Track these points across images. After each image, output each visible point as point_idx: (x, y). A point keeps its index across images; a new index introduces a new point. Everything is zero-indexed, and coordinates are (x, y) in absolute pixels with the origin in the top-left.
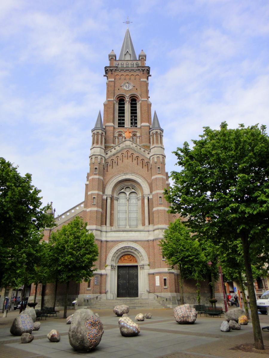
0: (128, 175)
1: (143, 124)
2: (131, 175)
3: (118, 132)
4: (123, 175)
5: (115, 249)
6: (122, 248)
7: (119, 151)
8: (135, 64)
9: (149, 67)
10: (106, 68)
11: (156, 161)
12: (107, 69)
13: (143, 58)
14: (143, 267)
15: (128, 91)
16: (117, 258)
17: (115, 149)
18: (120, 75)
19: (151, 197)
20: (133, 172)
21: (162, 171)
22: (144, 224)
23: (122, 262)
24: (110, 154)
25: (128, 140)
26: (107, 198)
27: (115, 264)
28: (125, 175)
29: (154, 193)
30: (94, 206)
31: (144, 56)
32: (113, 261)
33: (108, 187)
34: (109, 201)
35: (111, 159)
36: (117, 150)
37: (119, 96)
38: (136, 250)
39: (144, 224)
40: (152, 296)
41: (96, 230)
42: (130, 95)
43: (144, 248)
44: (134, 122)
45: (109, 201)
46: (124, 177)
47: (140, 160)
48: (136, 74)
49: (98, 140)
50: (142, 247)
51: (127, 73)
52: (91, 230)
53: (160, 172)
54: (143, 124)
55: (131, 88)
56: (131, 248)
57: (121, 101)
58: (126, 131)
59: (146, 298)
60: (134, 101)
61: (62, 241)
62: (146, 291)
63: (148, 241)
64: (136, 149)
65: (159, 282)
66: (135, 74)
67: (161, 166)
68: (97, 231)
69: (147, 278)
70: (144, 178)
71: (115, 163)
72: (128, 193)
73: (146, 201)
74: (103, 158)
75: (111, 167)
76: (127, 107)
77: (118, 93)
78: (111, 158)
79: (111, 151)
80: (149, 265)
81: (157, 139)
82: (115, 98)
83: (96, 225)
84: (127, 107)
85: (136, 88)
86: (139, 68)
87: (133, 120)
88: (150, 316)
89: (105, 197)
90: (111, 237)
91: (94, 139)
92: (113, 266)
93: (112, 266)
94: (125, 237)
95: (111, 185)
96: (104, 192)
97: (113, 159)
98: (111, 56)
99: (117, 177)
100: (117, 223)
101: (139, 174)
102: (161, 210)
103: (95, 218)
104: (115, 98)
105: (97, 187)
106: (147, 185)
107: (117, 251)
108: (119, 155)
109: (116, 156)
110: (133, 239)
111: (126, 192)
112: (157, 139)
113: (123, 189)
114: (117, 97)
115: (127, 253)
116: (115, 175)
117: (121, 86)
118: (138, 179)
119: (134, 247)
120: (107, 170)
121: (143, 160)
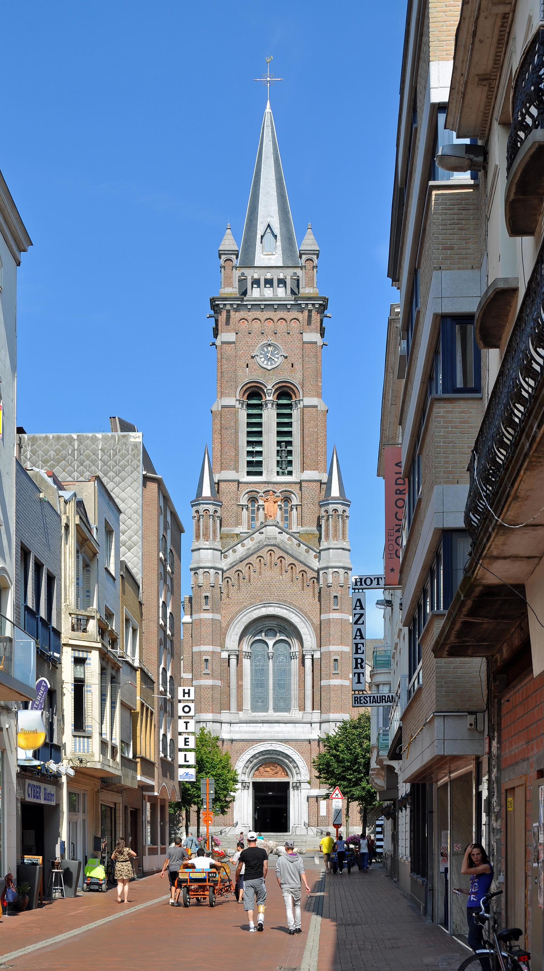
0: (271, 606)
1: (309, 474)
2: (279, 607)
3: (247, 493)
4: (262, 607)
5: (247, 753)
6: (261, 752)
7: (251, 552)
8: (289, 278)
9: (325, 298)
10: (213, 300)
11: (331, 582)
12: (216, 303)
13: (311, 260)
14: (297, 786)
15: (271, 372)
16: (252, 769)
17: (243, 546)
18: (250, 319)
19: (317, 655)
20: (282, 603)
21: (341, 606)
22: (392, 696)
23: (262, 776)
24: (232, 557)
25: (271, 523)
26: (229, 656)
27: (249, 779)
28: (264, 607)
29: (324, 649)
30: (207, 676)
31: (314, 254)
32: (245, 774)
33: (230, 633)
34: (233, 661)
35: (235, 570)
36: (249, 549)
37: (249, 385)
38: (287, 756)
39: (302, 708)
40: (313, 831)
41: (213, 722)
42: (277, 384)
43: (302, 753)
44: (284, 464)
45: (233, 661)
46: (264, 611)
47: (298, 571)
48: (291, 318)
49: (206, 528)
50: (298, 750)
51: (269, 314)
52: (203, 722)
53: (338, 607)
54: (309, 474)
55: (279, 361)
56: (278, 753)
57: (254, 393)
58: (267, 499)
59: (303, 834)
60: (285, 392)
61: (198, 732)
62: (303, 824)
63: (309, 741)
64: (288, 547)
65: (325, 810)
66: (289, 315)
67: (340, 593)
68: (215, 724)
69: (305, 805)
70: (306, 614)
71: (244, 579)
72: (271, 643)
73: (308, 662)
74: (220, 572)
75: (236, 587)
76: (270, 417)
77: (246, 377)
78: (236, 568)
79: (234, 551)
80: (309, 783)
81: (336, 530)
82: (238, 396)
83: (213, 712)
84: (270, 417)
85: (291, 360)
86: (299, 302)
87: (284, 454)
88: (304, 852)
89: (225, 655)
90: (241, 732)
91: (199, 526)
92: (246, 783)
93: (242, 783)
94: (265, 732)
95: (236, 629)
96: (222, 645)
97: (240, 569)
98: (224, 254)
99: (248, 611)
100: (68, 574)
101: (295, 606)
102: (335, 685)
103: (210, 700)
104: (238, 396)
105: (210, 638)
106: (311, 629)
107: (252, 757)
108: (253, 559)
109: (246, 562)
110: (281, 736)
111: (267, 641)
112: (336, 530)
113: (261, 632)
114: (244, 388)
115: (272, 759)
116: (245, 607)
117: (253, 357)
118: (294, 615)
119: (282, 751)
120: (228, 594)
121: (303, 572)
